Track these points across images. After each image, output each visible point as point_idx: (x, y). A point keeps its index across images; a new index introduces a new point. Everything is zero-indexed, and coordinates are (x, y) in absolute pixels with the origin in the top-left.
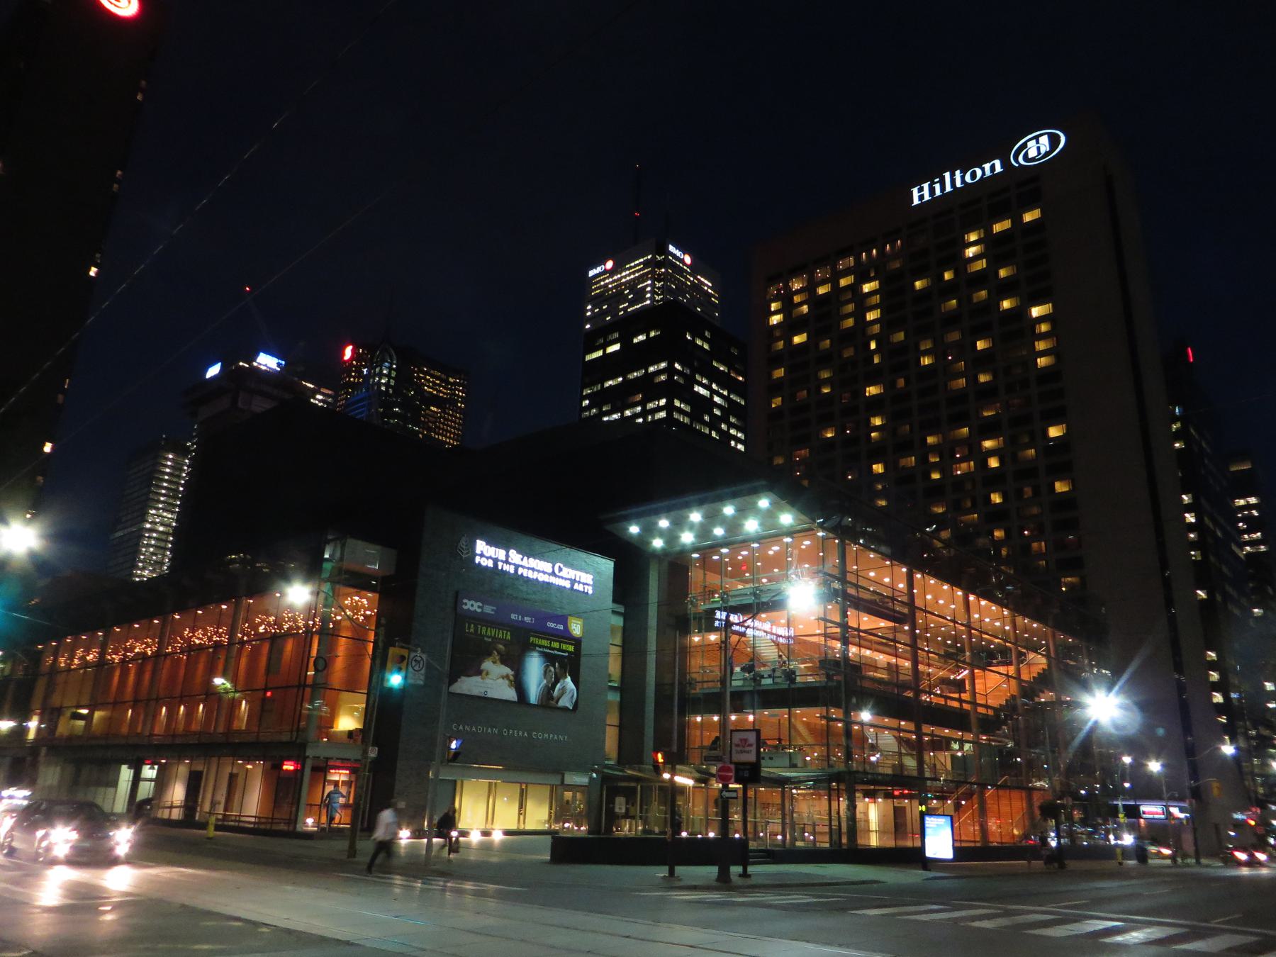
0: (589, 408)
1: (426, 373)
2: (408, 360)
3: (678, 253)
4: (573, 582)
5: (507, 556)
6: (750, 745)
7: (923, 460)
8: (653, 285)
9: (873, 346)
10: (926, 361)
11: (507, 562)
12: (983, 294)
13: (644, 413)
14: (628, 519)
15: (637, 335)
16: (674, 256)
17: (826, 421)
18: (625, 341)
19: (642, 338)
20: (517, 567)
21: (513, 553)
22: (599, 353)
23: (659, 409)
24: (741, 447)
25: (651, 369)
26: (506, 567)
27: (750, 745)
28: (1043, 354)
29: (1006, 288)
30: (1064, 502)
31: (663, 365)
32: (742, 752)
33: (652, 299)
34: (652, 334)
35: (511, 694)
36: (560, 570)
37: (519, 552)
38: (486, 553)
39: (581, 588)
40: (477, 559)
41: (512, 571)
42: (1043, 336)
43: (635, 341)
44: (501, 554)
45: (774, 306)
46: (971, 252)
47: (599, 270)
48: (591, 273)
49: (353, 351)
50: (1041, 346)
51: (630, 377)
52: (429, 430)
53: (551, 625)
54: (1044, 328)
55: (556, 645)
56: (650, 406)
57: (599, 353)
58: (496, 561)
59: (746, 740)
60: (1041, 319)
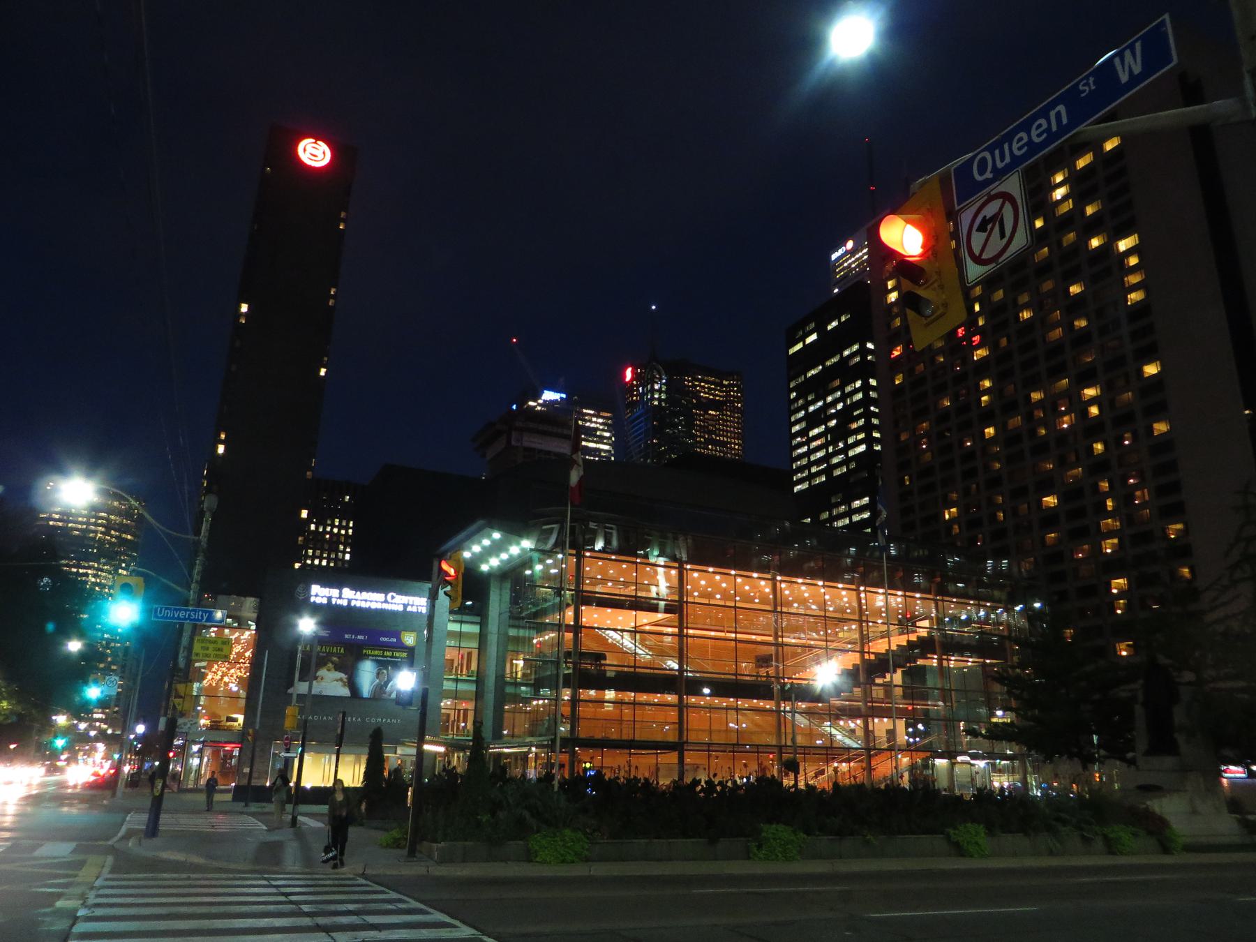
0: (796, 399)
1: (700, 381)
2: (676, 370)
4: (405, 606)
7: (1029, 417)
9: (977, 308)
10: (1026, 315)
11: (340, 597)
12: (1072, 236)
15: (830, 323)
17: (941, 390)
18: (820, 329)
19: (835, 324)
20: (350, 601)
22: (800, 346)
23: (856, 391)
25: (846, 353)
26: (340, 602)
28: (1134, 288)
29: (1093, 226)
30: (1165, 443)
31: (856, 347)
34: (843, 319)
35: (345, 692)
36: (393, 597)
40: (313, 599)
42: (1134, 270)
43: (829, 328)
44: (335, 592)
45: (890, 284)
46: (1059, 194)
47: (841, 252)
48: (834, 257)
49: (632, 372)
50: (1134, 279)
51: (828, 363)
52: (710, 433)
53: (382, 639)
54: (1133, 261)
55: (389, 654)
56: (848, 389)
57: (800, 346)
60: (1129, 252)
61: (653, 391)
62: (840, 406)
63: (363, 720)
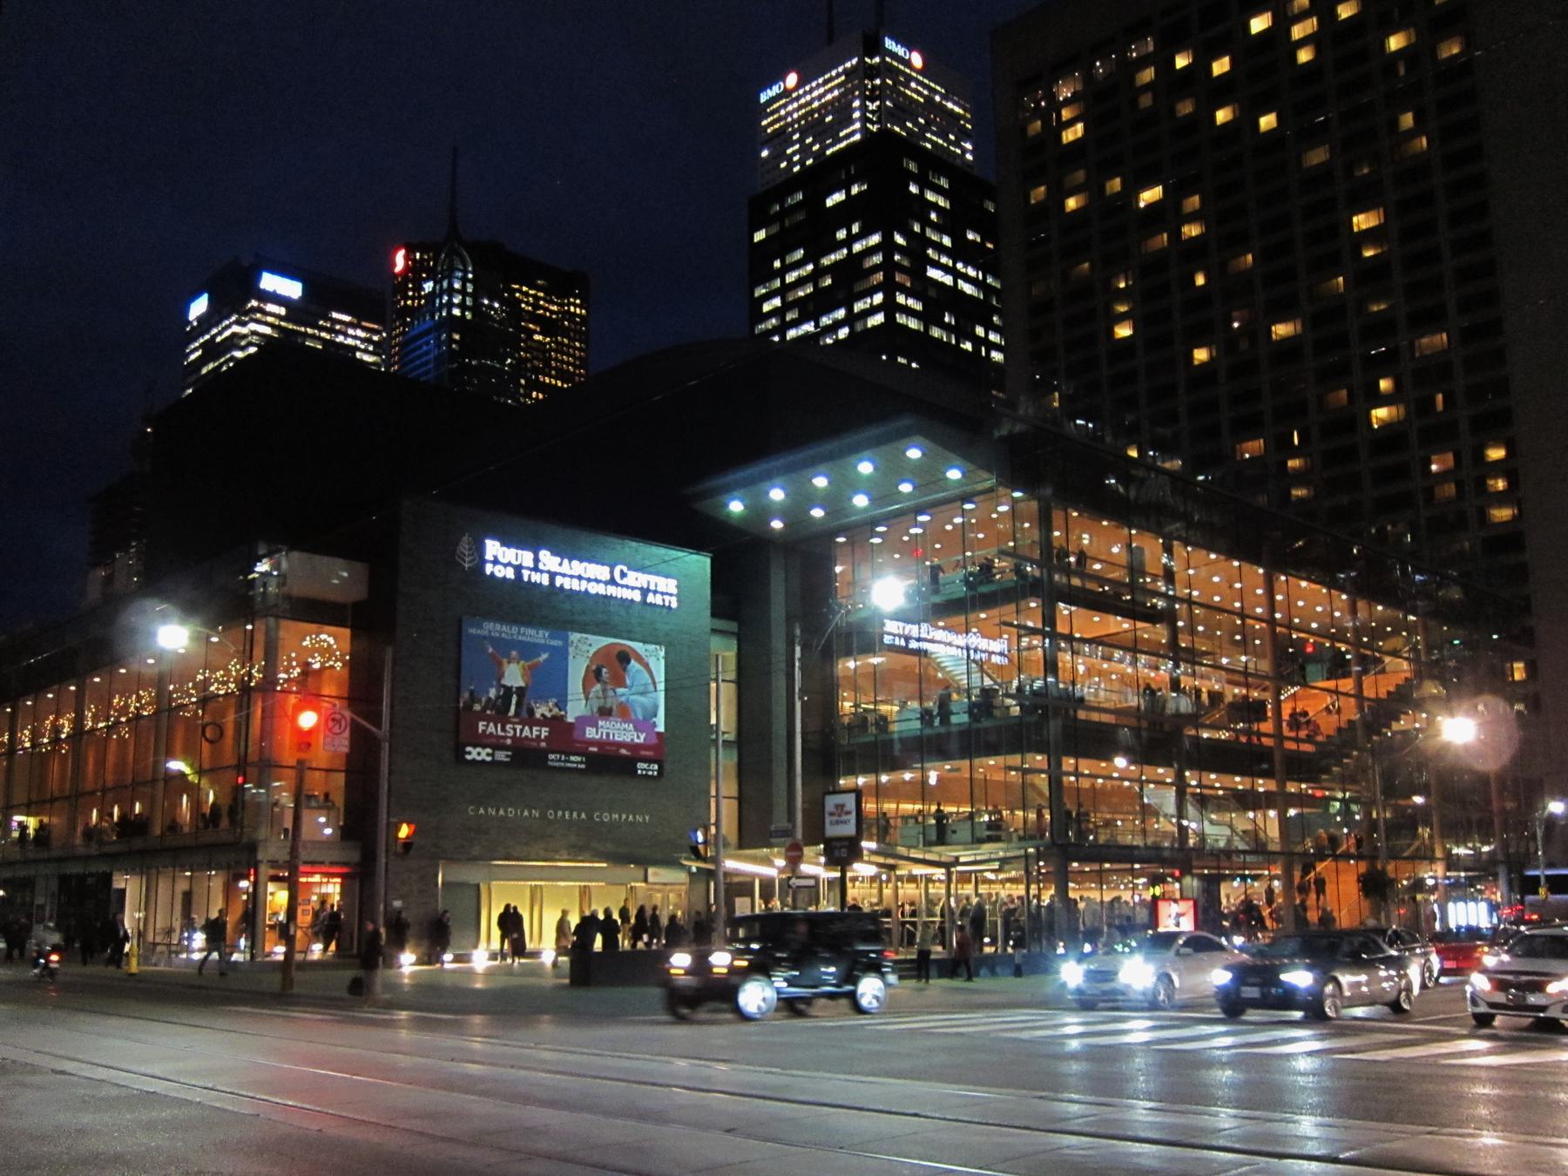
3: (900, 50)
4: (645, 592)
5: (536, 560)
6: (848, 813)
8: (863, 108)
11: (536, 569)
13: (850, 320)
14: (728, 489)
15: (830, 193)
16: (894, 56)
20: (553, 575)
21: (545, 555)
23: (873, 310)
24: (997, 356)
26: (536, 577)
27: (848, 813)
32: (837, 823)
33: (864, 130)
34: (855, 190)
36: (623, 575)
37: (554, 553)
38: (502, 558)
39: (658, 600)
40: (489, 569)
41: (546, 582)
43: (830, 202)
44: (526, 558)
48: (763, 98)
49: (407, 258)
58: (518, 569)
59: (842, 806)
61: (451, 291)
62: (843, 333)
63: (590, 817)
